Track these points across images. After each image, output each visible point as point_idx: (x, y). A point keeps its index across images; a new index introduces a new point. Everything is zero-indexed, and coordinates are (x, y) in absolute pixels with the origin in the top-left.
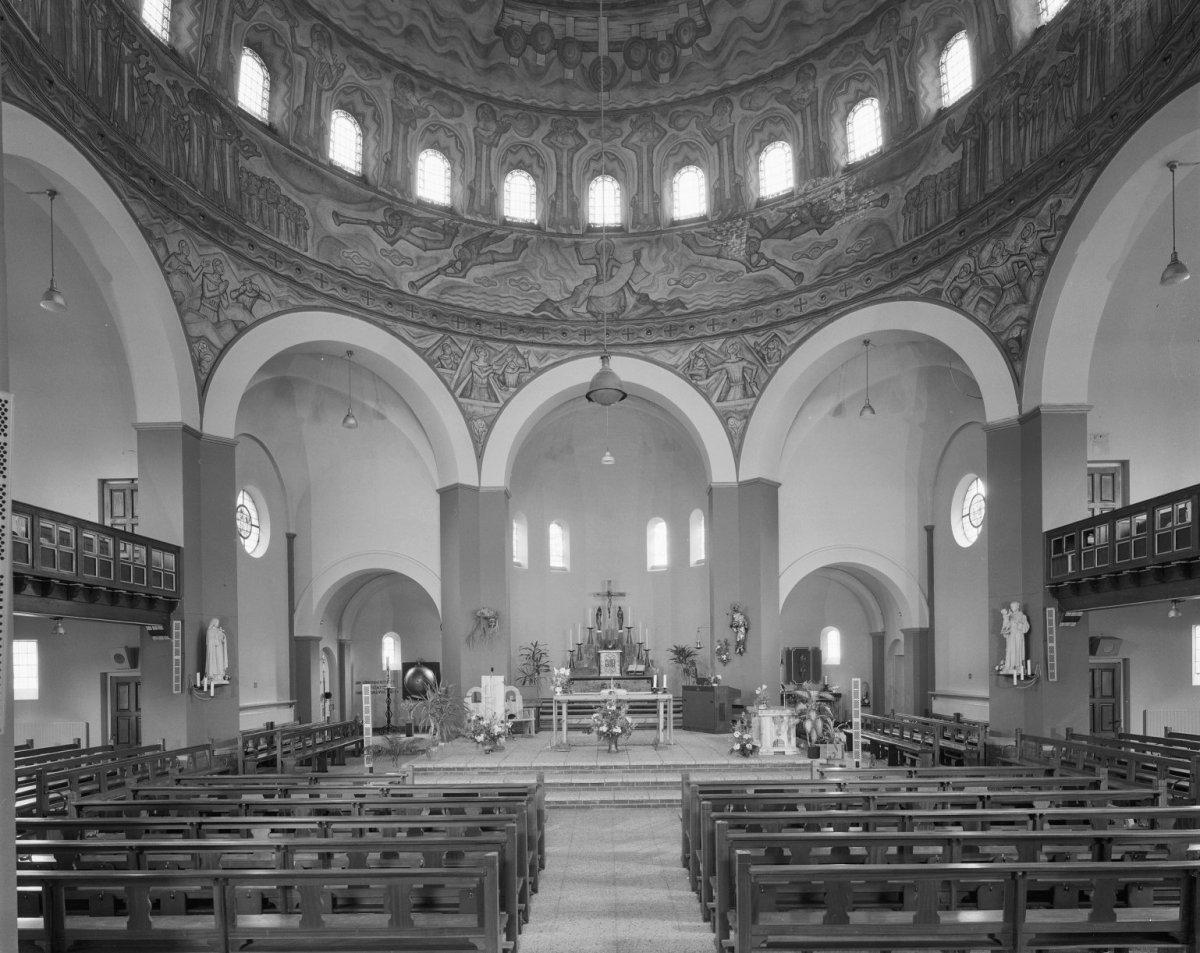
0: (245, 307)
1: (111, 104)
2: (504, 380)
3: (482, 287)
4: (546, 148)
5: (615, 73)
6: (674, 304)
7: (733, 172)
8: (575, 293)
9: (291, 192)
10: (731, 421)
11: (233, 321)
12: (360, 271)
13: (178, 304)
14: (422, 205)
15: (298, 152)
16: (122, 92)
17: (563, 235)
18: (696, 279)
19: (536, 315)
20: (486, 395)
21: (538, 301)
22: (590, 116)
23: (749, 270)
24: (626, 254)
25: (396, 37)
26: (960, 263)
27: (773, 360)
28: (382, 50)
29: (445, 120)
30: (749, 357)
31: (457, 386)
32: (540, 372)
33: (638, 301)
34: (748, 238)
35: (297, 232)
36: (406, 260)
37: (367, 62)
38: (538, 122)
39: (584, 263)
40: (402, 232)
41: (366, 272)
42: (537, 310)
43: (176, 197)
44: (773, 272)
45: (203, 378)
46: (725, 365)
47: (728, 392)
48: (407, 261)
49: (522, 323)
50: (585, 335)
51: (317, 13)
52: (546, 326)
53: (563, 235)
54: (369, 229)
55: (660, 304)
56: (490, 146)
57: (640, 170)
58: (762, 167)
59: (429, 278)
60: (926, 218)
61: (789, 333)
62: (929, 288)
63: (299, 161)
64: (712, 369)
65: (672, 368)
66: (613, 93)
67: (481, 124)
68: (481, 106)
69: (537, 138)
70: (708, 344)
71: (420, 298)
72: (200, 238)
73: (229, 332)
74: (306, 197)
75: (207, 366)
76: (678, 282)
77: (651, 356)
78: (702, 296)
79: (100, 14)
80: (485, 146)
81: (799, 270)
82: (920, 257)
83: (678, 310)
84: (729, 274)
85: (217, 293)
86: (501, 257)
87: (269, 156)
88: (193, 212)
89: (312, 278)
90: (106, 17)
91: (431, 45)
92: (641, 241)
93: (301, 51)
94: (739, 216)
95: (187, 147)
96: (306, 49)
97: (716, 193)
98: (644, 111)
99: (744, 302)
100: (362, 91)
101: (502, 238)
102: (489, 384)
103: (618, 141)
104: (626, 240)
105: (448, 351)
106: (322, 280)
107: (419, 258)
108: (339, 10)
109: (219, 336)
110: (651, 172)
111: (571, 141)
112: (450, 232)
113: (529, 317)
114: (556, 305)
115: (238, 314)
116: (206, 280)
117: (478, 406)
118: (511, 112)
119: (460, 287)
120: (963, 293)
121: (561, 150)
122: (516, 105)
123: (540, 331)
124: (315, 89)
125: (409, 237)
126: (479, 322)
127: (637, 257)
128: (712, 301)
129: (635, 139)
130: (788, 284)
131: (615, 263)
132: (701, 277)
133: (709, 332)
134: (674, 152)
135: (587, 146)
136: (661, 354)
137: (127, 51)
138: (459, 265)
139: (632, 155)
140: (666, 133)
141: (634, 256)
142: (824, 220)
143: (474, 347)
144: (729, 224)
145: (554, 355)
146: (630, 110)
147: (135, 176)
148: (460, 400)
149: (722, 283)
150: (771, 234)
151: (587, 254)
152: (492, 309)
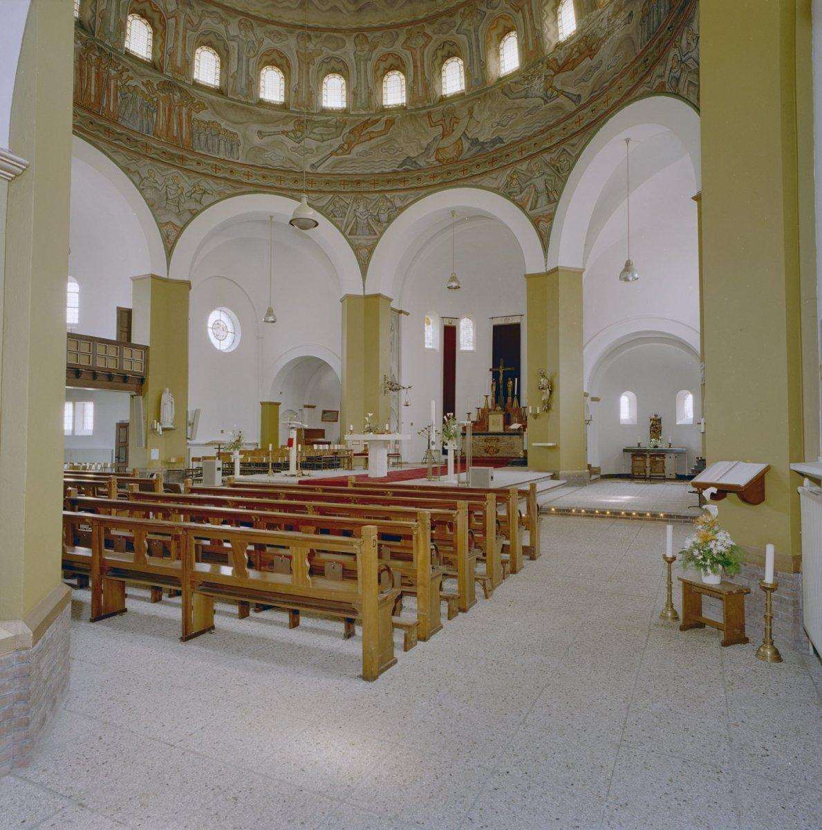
0: (196, 201)
1: (100, 104)
2: (379, 219)
4: (405, 50)
7: (534, 28)
9: (229, 126)
11: (189, 210)
12: (276, 164)
13: (151, 206)
15: (234, 100)
16: (109, 97)
17: (419, 109)
18: (511, 119)
19: (400, 169)
20: (368, 232)
21: (400, 160)
23: (546, 102)
25: (295, 9)
26: (671, 55)
27: (565, 170)
28: (287, 22)
29: (335, 53)
30: (547, 170)
31: (347, 227)
32: (402, 209)
33: (471, 144)
34: (546, 76)
35: (232, 148)
36: (308, 151)
37: (278, 32)
39: (433, 125)
41: (280, 164)
42: (401, 166)
43: (146, 146)
45: (170, 246)
46: (533, 180)
47: (537, 201)
48: (310, 151)
49: (390, 177)
50: (312, 184)
51: (241, 12)
52: (406, 176)
53: (419, 109)
54: (283, 137)
55: (486, 143)
56: (366, 60)
57: (471, 48)
60: (653, 22)
62: (657, 83)
63: (235, 105)
64: (524, 186)
65: (495, 190)
67: (359, 48)
68: (357, 36)
69: (398, 44)
71: (317, 173)
72: (162, 166)
73: (187, 216)
74: (240, 126)
75: (172, 238)
76: (498, 124)
79: (94, 57)
80: (362, 62)
81: (578, 93)
82: (650, 58)
83: (498, 145)
85: (177, 195)
87: (213, 108)
88: (158, 152)
89: (242, 175)
90: (99, 58)
91: (319, 7)
92: (473, 100)
93: (233, 39)
95: (155, 117)
96: (237, 36)
99: (542, 128)
100: (277, 51)
101: (377, 121)
102: (368, 222)
103: (453, 31)
105: (337, 206)
106: (248, 175)
107: (318, 148)
108: (254, 5)
109: (181, 220)
110: (478, 47)
111: (421, 41)
112: (340, 126)
113: (395, 172)
114: (414, 160)
115: (193, 205)
116: (168, 189)
118: (378, 34)
119: (346, 161)
120: (678, 80)
121: (415, 49)
123: (404, 180)
124: (244, 58)
125: (312, 135)
126: (358, 182)
128: (521, 133)
129: (465, 26)
130: (570, 106)
131: (456, 120)
132: (514, 116)
133: (519, 157)
134: (494, 26)
135: (433, 41)
136: (486, 181)
137: (113, 72)
138: (346, 147)
139: (464, 37)
141: (469, 111)
142: (594, 46)
143: (355, 200)
145: (411, 195)
147: (115, 140)
148: (349, 237)
149: (527, 117)
150: (561, 69)
151: (435, 118)
152: (369, 172)
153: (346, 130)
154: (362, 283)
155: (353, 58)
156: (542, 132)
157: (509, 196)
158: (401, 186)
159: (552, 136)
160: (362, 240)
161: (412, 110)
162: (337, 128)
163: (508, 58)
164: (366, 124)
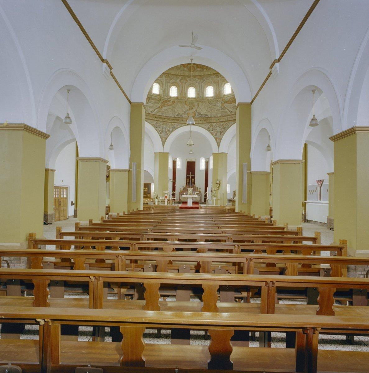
3: (166, 111)
5: (194, 69)
6: (206, 115)
8: (185, 112)
10: (217, 140)
14: (154, 94)
22: (189, 77)
24: (196, 104)
31: (159, 131)
32: (177, 128)
34: (222, 103)
38: (178, 78)
40: (150, 101)
42: (177, 115)
44: (226, 110)
47: (217, 134)
58: (225, 88)
59: (155, 110)
61: (229, 123)
66: (194, 72)
69: (178, 80)
70: (213, 124)
77: (200, 126)
78: (211, 114)
83: (207, 116)
84: (218, 110)
86: (169, 105)
94: (220, 98)
97: (215, 93)
98: (200, 76)
103: (195, 81)
104: (196, 101)
105: (158, 125)
111: (185, 81)
113: (175, 117)
117: (163, 135)
118: (173, 76)
122: (174, 75)
123: (177, 120)
126: (164, 119)
127: (198, 105)
129: (198, 81)
133: (213, 121)
136: (203, 125)
138: (161, 107)
140: (205, 80)
143: (163, 124)
144: (218, 99)
145: (180, 125)
146: (197, 76)
150: (226, 102)
151: (188, 104)
153: (161, 102)
154: (162, 148)
155: (164, 81)
156: (220, 117)
157: (209, 131)
158: (177, 122)
159: (223, 119)
160: (163, 135)
161: (180, 100)
162: (158, 101)
163: (210, 92)
164: (166, 101)
